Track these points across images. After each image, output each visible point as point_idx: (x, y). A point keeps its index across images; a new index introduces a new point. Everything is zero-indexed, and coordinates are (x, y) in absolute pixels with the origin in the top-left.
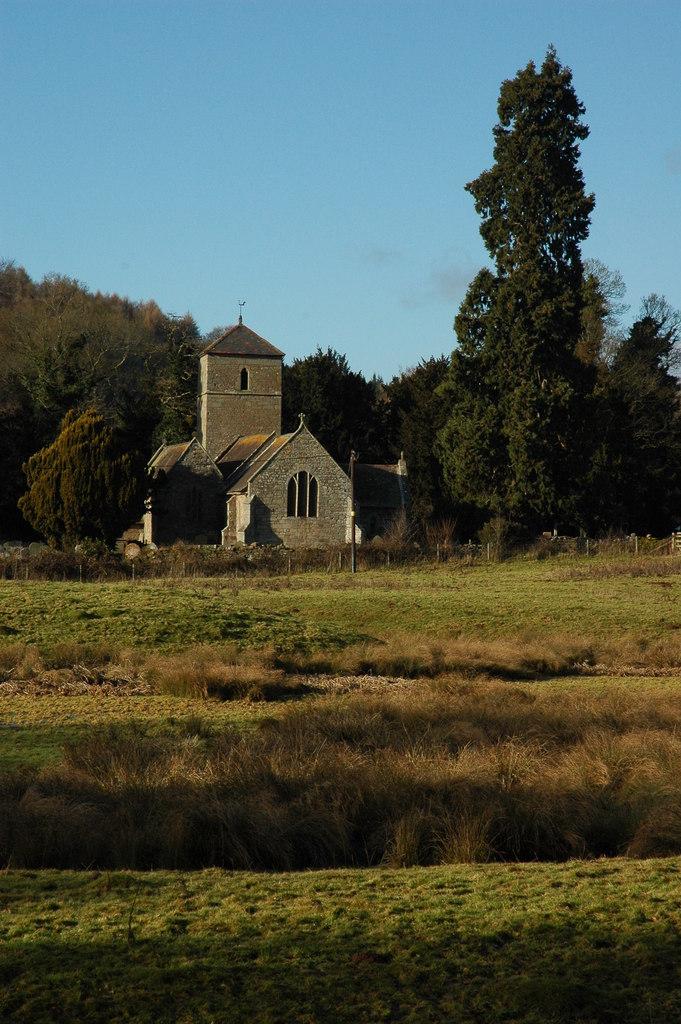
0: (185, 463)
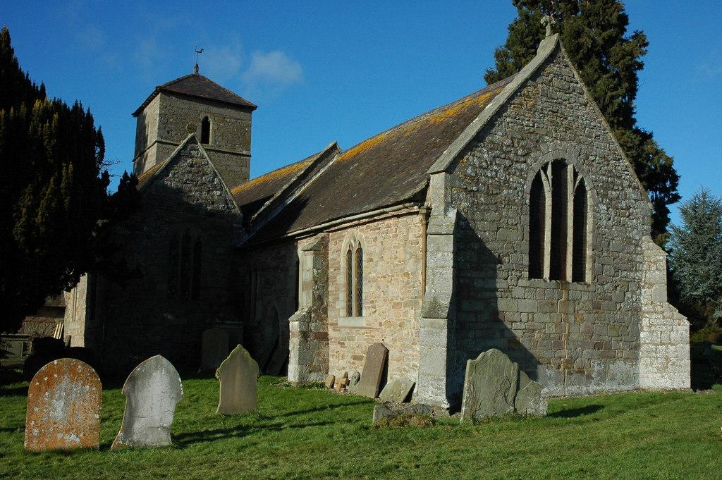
0: (171, 182)
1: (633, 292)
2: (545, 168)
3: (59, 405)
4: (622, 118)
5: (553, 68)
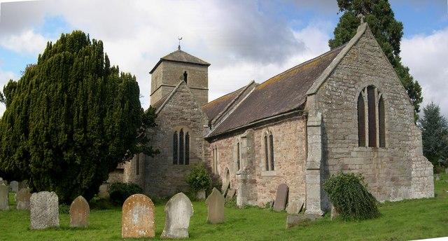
1: (408, 151)
2: (364, 90)
3: (136, 216)
4: (395, 63)
5: (363, 39)
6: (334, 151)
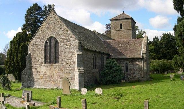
6: (34, 66)
